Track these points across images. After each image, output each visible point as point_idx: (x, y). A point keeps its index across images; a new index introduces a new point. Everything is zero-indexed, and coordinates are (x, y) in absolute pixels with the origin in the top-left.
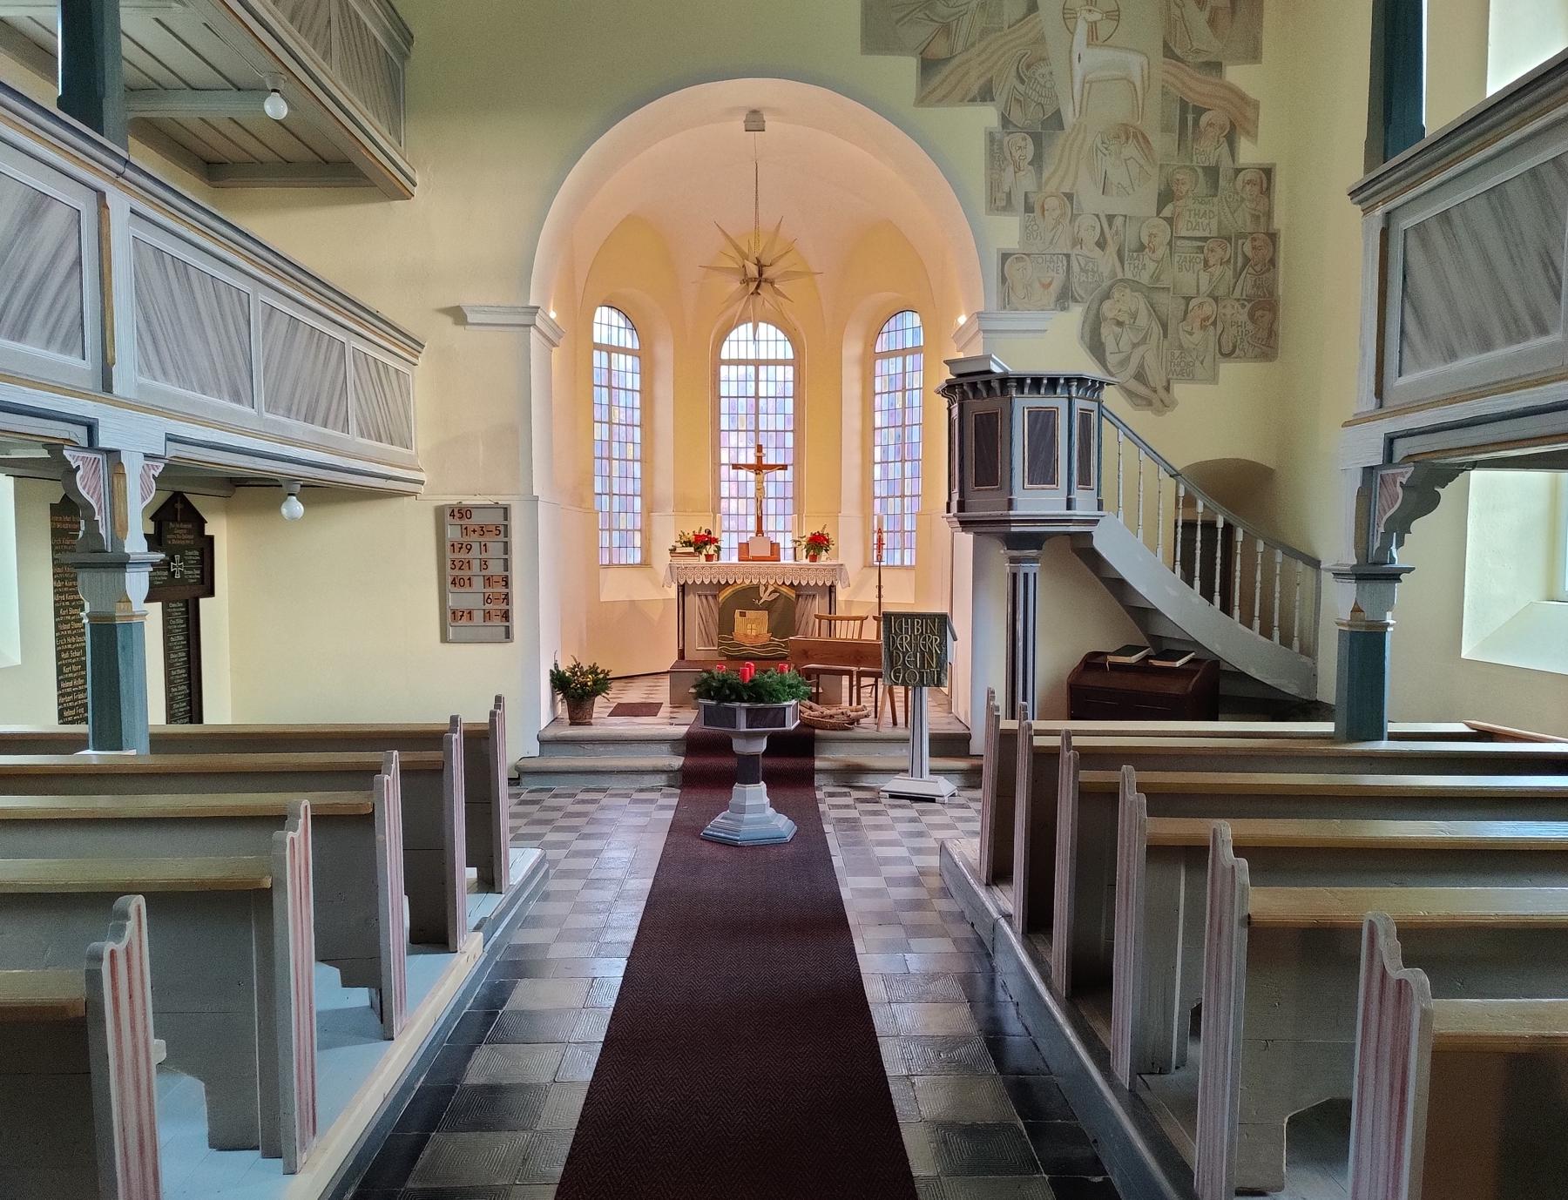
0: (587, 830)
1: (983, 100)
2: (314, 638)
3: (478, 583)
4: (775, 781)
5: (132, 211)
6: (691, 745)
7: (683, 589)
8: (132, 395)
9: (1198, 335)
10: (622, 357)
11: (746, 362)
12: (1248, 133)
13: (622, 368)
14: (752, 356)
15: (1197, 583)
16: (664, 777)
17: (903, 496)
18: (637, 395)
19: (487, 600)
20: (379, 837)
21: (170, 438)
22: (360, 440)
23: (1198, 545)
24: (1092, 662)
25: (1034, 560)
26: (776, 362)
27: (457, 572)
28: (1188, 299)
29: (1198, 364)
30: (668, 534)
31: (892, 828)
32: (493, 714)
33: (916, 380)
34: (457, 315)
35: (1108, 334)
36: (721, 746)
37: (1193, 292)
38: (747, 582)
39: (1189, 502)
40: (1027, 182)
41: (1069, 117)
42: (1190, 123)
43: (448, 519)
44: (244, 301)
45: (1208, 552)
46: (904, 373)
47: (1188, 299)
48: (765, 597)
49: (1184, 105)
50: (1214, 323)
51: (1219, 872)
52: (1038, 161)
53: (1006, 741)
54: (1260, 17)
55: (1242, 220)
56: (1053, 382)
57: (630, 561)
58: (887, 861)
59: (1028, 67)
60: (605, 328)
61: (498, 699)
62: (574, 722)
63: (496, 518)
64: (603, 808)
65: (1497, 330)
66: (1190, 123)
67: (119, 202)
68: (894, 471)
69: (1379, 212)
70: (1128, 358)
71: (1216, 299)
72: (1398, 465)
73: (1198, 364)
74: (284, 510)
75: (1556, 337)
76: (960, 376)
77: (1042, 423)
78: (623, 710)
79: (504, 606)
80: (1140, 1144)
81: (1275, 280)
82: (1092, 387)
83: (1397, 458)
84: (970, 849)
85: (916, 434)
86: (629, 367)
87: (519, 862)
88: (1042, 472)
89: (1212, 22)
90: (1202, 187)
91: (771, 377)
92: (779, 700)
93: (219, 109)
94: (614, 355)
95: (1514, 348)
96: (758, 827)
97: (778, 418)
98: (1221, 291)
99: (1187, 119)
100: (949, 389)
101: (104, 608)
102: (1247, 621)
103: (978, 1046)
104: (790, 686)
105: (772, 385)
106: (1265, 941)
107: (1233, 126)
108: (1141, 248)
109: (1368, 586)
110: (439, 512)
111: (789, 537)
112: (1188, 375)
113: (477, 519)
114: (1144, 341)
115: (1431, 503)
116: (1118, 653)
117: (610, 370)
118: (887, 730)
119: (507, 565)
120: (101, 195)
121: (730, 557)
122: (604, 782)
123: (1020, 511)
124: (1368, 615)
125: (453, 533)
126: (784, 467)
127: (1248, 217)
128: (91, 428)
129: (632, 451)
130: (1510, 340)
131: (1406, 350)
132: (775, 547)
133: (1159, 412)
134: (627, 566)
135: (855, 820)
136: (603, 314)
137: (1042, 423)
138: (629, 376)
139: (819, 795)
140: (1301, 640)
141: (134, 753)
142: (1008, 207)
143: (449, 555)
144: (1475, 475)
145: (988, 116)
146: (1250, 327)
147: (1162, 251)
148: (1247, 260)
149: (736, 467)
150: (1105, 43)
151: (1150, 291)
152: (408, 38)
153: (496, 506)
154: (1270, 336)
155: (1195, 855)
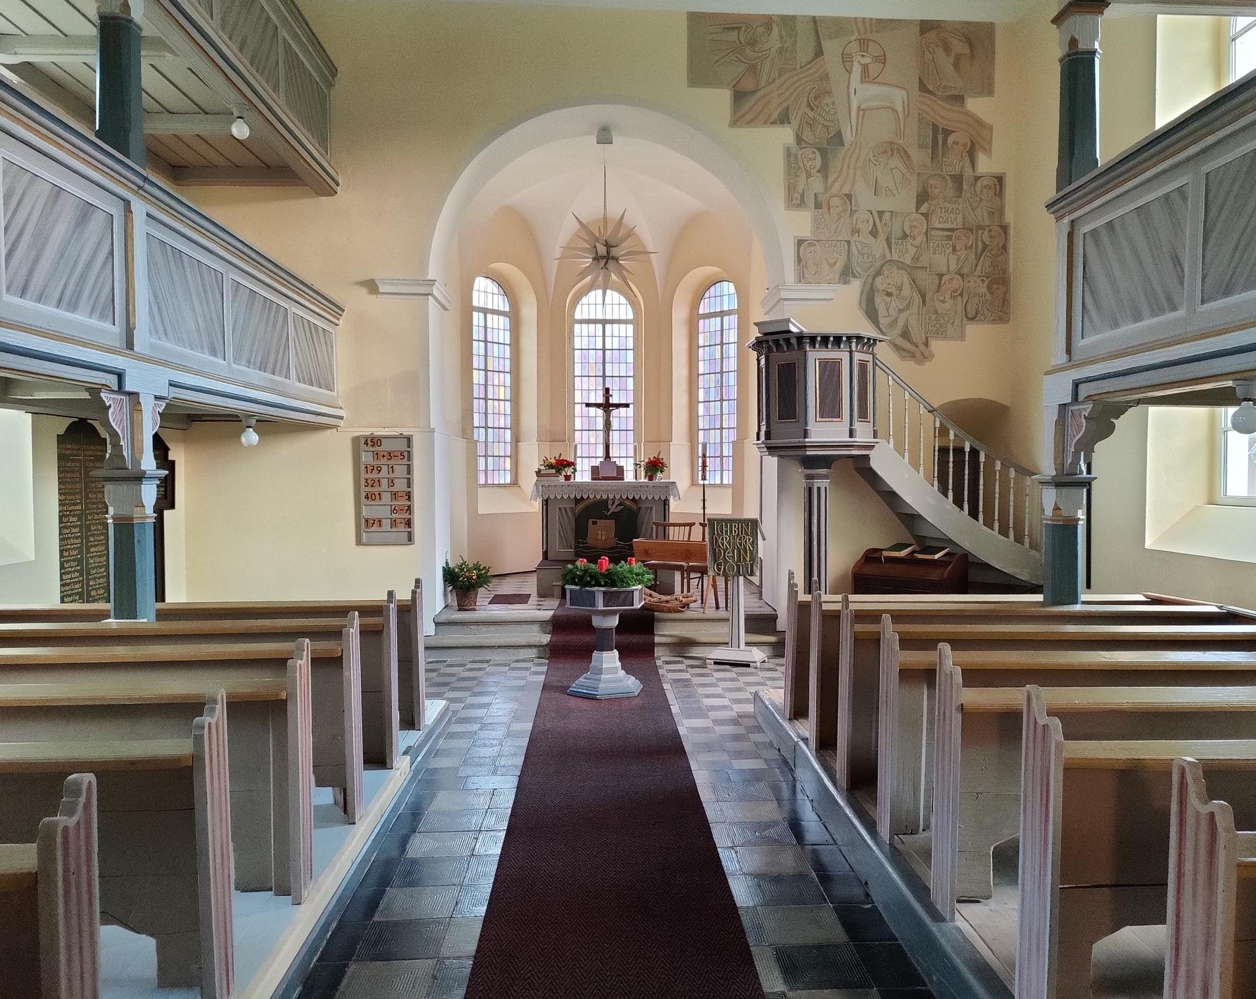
0: (478, 690)
1: (782, 123)
2: (255, 538)
3: (386, 498)
4: (626, 654)
5: (148, 215)
6: (557, 625)
7: (546, 503)
8: (147, 352)
9: (949, 302)
10: (496, 317)
11: (595, 322)
12: (985, 149)
13: (496, 326)
14: (600, 317)
15: (950, 494)
16: (535, 650)
17: (721, 428)
18: (508, 348)
19: (394, 511)
20: (346, 674)
21: (172, 384)
22: (297, 384)
23: (951, 464)
24: (871, 557)
25: (826, 477)
26: (619, 322)
27: (369, 489)
28: (941, 276)
29: (949, 325)
30: (532, 459)
31: (717, 685)
32: (414, 592)
33: (732, 336)
34: (371, 286)
35: (880, 301)
36: (584, 625)
37: (944, 270)
38: (598, 497)
39: (943, 432)
40: (817, 185)
41: (848, 136)
42: (940, 143)
43: (363, 446)
44: (219, 277)
45: (960, 471)
46: (722, 330)
47: (941, 276)
48: (613, 509)
49: (935, 128)
50: (961, 294)
51: (943, 679)
52: (824, 169)
53: (803, 608)
54: (992, 63)
55: (981, 215)
56: (838, 340)
57: (502, 482)
58: (713, 708)
59: (816, 98)
60: (482, 294)
61: (418, 582)
62: (461, 608)
63: (402, 446)
64: (488, 674)
65: (1146, 312)
66: (940, 143)
67: (139, 208)
68: (715, 408)
69: (1066, 220)
70: (895, 321)
71: (962, 276)
72: (1080, 403)
73: (949, 325)
74: (243, 439)
75: (1181, 313)
76: (766, 334)
77: (830, 372)
78: (498, 599)
79: (407, 516)
80: (895, 876)
81: (1007, 261)
82: (868, 343)
83: (1081, 398)
84: (777, 694)
85: (732, 379)
86: (501, 326)
87: (431, 710)
88: (830, 409)
89: (956, 66)
90: (950, 192)
91: (616, 334)
92: (629, 585)
93: (187, 128)
94: (489, 316)
95: (1155, 320)
96: (613, 685)
97: (623, 367)
98: (966, 270)
99: (938, 138)
100: (759, 345)
101: (124, 512)
102: (989, 523)
103: (783, 829)
104: (637, 575)
105: (616, 340)
106: (972, 719)
107: (973, 145)
108: (905, 236)
109: (1065, 490)
110: (356, 441)
111: (632, 461)
112: (941, 333)
113: (386, 446)
114: (908, 307)
115: (1109, 430)
116: (892, 549)
117: (486, 328)
118: (711, 612)
119: (409, 484)
120: (127, 203)
121: (583, 475)
122: (487, 655)
123: (813, 438)
124: (1065, 512)
125: (366, 458)
126: (627, 406)
127: (986, 213)
128: (120, 376)
129: (503, 393)
130: (1154, 314)
131: (1086, 322)
132: (620, 470)
133: (920, 363)
134: (499, 485)
135: (687, 680)
136: (481, 283)
137: (830, 372)
138: (501, 332)
139: (659, 663)
140: (1030, 536)
141: (146, 620)
142: (801, 204)
143: (364, 475)
144: (1153, 410)
145: (786, 135)
146: (988, 297)
147: (921, 239)
148: (985, 247)
149: (588, 405)
150: (874, 81)
151: (911, 270)
152: (334, 71)
153: (401, 436)
154: (1004, 304)
155: (929, 676)
